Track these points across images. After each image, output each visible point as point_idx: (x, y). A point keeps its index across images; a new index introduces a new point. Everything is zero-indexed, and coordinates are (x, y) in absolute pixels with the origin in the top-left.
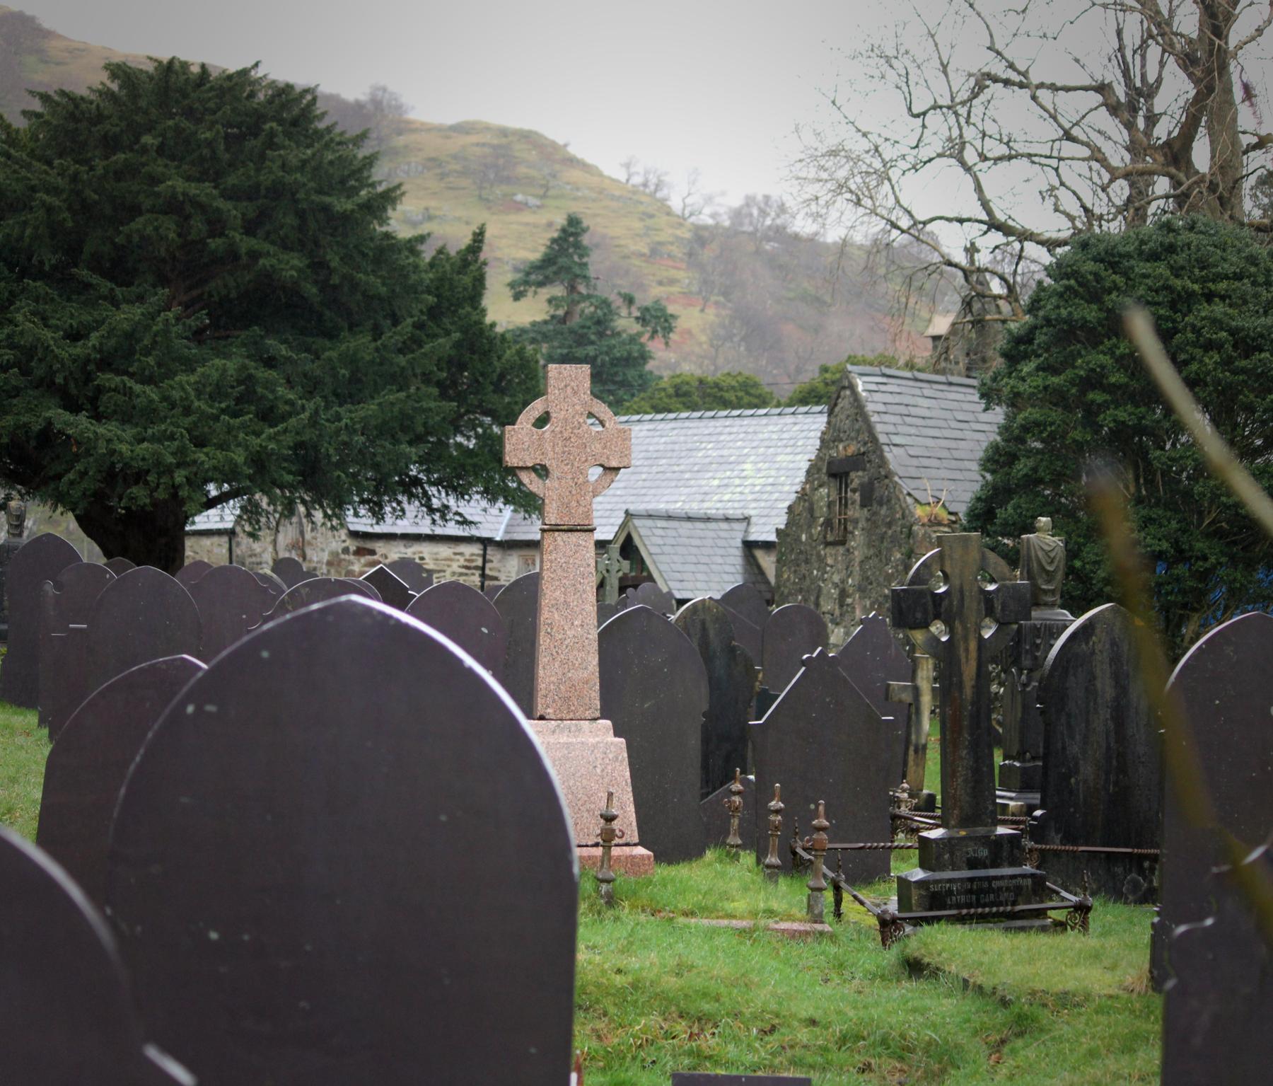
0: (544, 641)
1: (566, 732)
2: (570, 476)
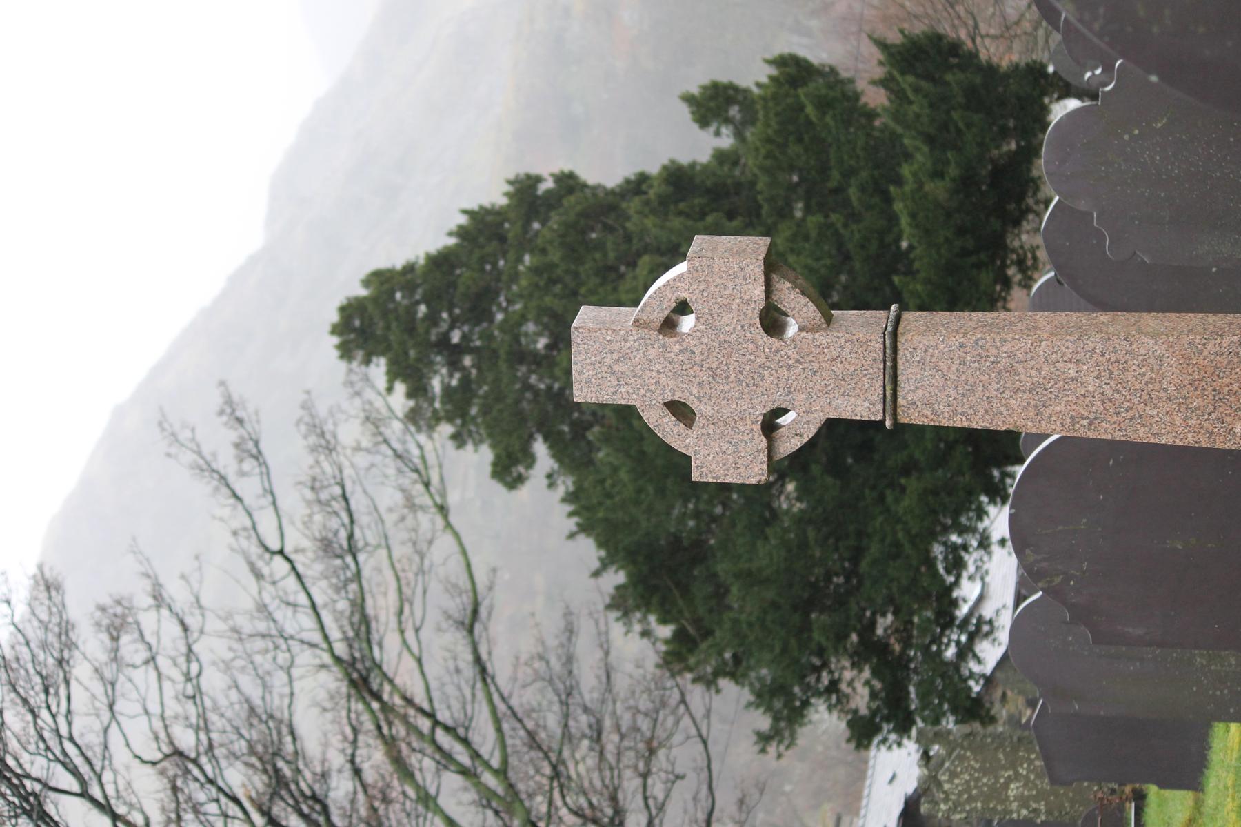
0: (1107, 431)
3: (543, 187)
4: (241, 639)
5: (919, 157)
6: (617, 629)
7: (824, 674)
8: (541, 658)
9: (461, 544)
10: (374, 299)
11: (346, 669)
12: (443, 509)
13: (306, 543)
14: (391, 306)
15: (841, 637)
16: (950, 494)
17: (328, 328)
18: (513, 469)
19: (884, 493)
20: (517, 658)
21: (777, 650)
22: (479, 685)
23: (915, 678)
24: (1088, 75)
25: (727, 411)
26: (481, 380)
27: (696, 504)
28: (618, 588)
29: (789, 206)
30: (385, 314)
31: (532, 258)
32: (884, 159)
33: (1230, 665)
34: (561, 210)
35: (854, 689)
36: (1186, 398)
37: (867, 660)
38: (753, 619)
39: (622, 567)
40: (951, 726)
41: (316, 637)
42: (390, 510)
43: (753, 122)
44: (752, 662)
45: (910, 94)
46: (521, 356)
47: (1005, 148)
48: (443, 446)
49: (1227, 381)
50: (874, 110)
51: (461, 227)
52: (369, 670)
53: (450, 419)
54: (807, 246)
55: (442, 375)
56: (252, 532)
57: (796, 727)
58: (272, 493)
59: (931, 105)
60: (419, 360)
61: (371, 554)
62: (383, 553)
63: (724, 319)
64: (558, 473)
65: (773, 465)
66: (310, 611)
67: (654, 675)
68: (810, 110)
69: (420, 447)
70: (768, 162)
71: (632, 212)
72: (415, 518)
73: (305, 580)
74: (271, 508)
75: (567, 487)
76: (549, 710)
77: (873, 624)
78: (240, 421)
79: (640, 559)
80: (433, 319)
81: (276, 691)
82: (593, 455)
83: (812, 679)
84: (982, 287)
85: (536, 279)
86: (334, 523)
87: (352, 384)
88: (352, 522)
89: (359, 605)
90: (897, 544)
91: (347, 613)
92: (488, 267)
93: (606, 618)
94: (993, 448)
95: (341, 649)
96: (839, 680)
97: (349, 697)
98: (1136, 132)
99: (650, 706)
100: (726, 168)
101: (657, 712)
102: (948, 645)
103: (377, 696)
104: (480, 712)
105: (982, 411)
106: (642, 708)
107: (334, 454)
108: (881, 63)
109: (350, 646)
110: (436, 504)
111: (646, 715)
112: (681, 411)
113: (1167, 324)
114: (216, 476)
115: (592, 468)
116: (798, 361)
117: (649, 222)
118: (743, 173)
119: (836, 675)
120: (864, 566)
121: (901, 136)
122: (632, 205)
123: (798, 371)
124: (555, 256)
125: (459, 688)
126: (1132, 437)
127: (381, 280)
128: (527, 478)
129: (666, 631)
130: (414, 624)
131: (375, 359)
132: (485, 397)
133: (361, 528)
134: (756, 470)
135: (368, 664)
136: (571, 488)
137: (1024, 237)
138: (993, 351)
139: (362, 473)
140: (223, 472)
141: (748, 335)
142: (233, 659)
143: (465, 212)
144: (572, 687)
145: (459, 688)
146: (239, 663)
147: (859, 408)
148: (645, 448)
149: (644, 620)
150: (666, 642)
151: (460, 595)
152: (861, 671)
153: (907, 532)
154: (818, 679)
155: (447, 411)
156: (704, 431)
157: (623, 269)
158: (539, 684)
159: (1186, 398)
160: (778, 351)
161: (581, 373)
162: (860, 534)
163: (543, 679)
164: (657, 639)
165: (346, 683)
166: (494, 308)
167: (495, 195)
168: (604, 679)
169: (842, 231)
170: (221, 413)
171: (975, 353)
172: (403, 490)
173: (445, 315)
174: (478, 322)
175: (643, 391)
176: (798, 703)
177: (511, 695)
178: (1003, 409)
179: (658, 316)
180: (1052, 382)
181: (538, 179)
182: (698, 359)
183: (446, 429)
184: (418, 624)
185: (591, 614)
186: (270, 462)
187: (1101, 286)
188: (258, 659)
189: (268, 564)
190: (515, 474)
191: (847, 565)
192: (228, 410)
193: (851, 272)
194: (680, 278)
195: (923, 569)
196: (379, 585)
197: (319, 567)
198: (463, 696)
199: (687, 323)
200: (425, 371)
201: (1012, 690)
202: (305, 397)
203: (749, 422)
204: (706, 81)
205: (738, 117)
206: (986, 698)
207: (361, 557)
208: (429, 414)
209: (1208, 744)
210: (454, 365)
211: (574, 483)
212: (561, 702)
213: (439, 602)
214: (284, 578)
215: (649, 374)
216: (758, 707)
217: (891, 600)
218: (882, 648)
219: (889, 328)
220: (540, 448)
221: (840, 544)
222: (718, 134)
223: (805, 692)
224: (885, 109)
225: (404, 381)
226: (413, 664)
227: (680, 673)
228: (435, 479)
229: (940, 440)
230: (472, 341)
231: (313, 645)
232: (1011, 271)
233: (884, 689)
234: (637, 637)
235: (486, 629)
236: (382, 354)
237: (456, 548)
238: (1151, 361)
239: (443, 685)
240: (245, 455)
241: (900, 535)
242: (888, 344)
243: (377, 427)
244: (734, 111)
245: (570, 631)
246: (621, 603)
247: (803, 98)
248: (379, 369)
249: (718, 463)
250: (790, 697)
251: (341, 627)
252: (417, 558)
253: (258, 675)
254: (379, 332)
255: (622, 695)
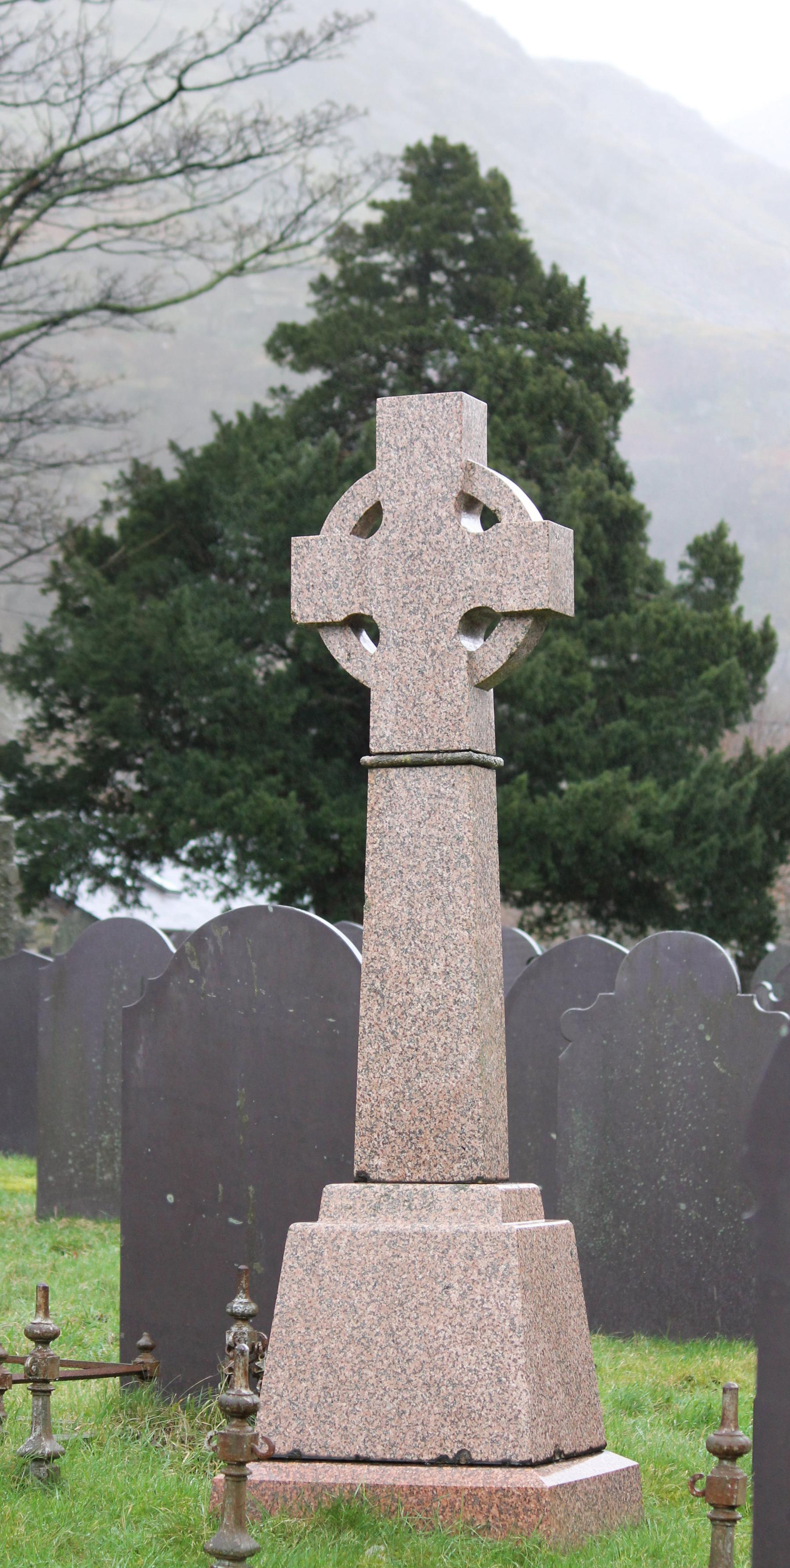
0: (369, 1010)
1: (403, 1211)
2: (420, 637)
3: (612, 369)
4: (77, 45)
5: (664, 799)
6: (110, 473)
7: (70, 712)
8: (73, 388)
9: (200, 292)
10: (476, 183)
11: (48, 166)
12: (239, 270)
13: (192, 116)
14: (469, 203)
15: (114, 730)
16: (280, 848)
17: (441, 133)
18: (289, 348)
19: (282, 768)
20: (71, 361)
21: (95, 657)
22: (38, 319)
23: (70, 816)
24: (768, 986)
25: (373, 574)
26: (390, 308)
27: (257, 558)
28: (158, 473)
29: (606, 651)
30: (460, 197)
31: (532, 360)
32: (658, 758)
33: (102, 1174)
34: (586, 391)
35: (54, 747)
36: (410, 1100)
37: (88, 760)
38: (130, 628)
39: (183, 476)
40: (16, 860)
41: (84, 131)
42: (236, 210)
43: (697, 607)
44: (80, 629)
45: (738, 785)
46: (418, 349)
47: (678, 896)
48: (312, 268)
49: (432, 1146)
50: (717, 745)
51: (565, 279)
52: (49, 192)
53: (343, 274)
54: (559, 673)
55: (393, 263)
56: (202, 55)
57: (7, 683)
58: (248, 76)
59: (724, 812)
60: (409, 236)
61: (184, 190)
62: (186, 204)
63: (478, 567)
64: (288, 399)
65: (312, 631)
66: (114, 123)
67: (59, 518)
68: (714, 671)
69: (310, 242)
70: (652, 626)
71: (589, 471)
72: (228, 239)
73: (150, 116)
74: (230, 75)
75: (272, 410)
76: (12, 400)
77: (127, 767)
78: (329, 37)
79: (194, 496)
80: (457, 250)
81: (20, 87)
82: (308, 438)
83: (63, 698)
84: (518, 876)
85: (508, 364)
86: (217, 147)
87: (378, 161)
88: (220, 168)
89: (124, 178)
90: (220, 791)
91: (114, 166)
92: (519, 310)
93: (124, 460)
94: (338, 886)
95: (72, 159)
96: (64, 730)
97: (17, 170)
98: (708, 1038)
99: (23, 515)
100: (642, 576)
101: (17, 523)
102: (109, 854)
103: (19, 202)
104: (7, 321)
105: (385, 866)
106: (20, 506)
107: (296, 145)
108: (769, 751)
109: (75, 170)
110: (244, 262)
111: (12, 511)
112: (370, 522)
113: (494, 1075)
114: (265, 12)
115: (293, 437)
116: (434, 653)
117: (578, 492)
118: (639, 597)
119: (69, 726)
120: (195, 754)
121: (688, 777)
122: (597, 471)
123: (423, 653)
124: (535, 385)
125: (33, 296)
126: (363, 1041)
127: (498, 191)
128: (280, 364)
129: (111, 529)
130: (105, 242)
131: (408, 187)
132: (371, 313)
133: (213, 178)
134: (307, 610)
135: (56, 191)
136: (271, 415)
137: (576, 924)
138: (454, 875)
139: (277, 177)
140: (270, 19)
141: (462, 594)
142: (54, 37)
143: (583, 282)
144: (40, 424)
145: (33, 296)
146: (50, 45)
147: (382, 725)
148: (318, 497)
149: (123, 503)
150: (99, 530)
151: (141, 293)
152: (76, 754)
153: (236, 801)
154: (63, 706)
155: (352, 270)
156: (349, 548)
157: (523, 463)
158: (42, 386)
159: (410, 1100)
160: (445, 629)
161: (410, 405)
162: (230, 748)
163: (48, 391)
164: (101, 519)
165: (32, 166)
166: (471, 318)
167: (601, 316)
168: (52, 461)
169: (576, 713)
170: (338, 16)
171: (452, 855)
172: (259, 224)
173: (462, 264)
174: (454, 302)
175: (392, 477)
176: (34, 683)
177: (27, 355)
178: (389, 890)
179: (478, 491)
180: (422, 945)
181: (622, 364)
182: (432, 538)
183: (332, 270)
184: (106, 246)
185: (127, 442)
186: (284, 73)
187: (531, 1005)
188: (56, 66)
189: (167, 74)
190: (284, 350)
191: (194, 734)
192: (341, 24)
193: (530, 725)
194: (523, 514)
195: (193, 822)
196: (148, 200)
197: (166, 132)
198: (24, 301)
199: (472, 524)
200: (397, 244)
201: (60, 930)
202: (361, 110)
203: (362, 599)
204: (742, 551)
205: (702, 589)
206: (49, 901)
207: (179, 179)
208: (348, 250)
209: (11, 1154)
210: (406, 277)
211: (277, 418)
212: (22, 413)
213: (132, 270)
214: (151, 92)
215: (411, 482)
216: (28, 638)
217: (156, 786)
218: (101, 779)
219: (475, 756)
220: (315, 377)
221: (219, 726)
222: (683, 566)
223: (48, 690)
224: (717, 758)
225: (385, 221)
226: (59, 242)
227: (64, 547)
228: (273, 260)
229: (342, 835)
230: (434, 296)
231: (74, 128)
232: (537, 910)
233: (56, 781)
234: (102, 497)
235: (104, 324)
236: (415, 195)
237: (195, 287)
238: (451, 1057)
239: (36, 277)
240: (291, 44)
241: (232, 794)
242: (458, 755)
243: (330, 192)
244: (709, 584)
245: (106, 420)
246: (141, 476)
247: (727, 662)
248: (396, 192)
249: (313, 566)
250: (41, 674)
251: (97, 159)
252: (181, 242)
253: (37, 66)
254: (439, 190)
255: (34, 482)
